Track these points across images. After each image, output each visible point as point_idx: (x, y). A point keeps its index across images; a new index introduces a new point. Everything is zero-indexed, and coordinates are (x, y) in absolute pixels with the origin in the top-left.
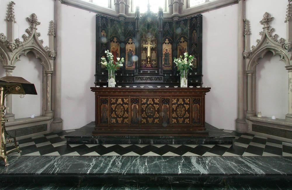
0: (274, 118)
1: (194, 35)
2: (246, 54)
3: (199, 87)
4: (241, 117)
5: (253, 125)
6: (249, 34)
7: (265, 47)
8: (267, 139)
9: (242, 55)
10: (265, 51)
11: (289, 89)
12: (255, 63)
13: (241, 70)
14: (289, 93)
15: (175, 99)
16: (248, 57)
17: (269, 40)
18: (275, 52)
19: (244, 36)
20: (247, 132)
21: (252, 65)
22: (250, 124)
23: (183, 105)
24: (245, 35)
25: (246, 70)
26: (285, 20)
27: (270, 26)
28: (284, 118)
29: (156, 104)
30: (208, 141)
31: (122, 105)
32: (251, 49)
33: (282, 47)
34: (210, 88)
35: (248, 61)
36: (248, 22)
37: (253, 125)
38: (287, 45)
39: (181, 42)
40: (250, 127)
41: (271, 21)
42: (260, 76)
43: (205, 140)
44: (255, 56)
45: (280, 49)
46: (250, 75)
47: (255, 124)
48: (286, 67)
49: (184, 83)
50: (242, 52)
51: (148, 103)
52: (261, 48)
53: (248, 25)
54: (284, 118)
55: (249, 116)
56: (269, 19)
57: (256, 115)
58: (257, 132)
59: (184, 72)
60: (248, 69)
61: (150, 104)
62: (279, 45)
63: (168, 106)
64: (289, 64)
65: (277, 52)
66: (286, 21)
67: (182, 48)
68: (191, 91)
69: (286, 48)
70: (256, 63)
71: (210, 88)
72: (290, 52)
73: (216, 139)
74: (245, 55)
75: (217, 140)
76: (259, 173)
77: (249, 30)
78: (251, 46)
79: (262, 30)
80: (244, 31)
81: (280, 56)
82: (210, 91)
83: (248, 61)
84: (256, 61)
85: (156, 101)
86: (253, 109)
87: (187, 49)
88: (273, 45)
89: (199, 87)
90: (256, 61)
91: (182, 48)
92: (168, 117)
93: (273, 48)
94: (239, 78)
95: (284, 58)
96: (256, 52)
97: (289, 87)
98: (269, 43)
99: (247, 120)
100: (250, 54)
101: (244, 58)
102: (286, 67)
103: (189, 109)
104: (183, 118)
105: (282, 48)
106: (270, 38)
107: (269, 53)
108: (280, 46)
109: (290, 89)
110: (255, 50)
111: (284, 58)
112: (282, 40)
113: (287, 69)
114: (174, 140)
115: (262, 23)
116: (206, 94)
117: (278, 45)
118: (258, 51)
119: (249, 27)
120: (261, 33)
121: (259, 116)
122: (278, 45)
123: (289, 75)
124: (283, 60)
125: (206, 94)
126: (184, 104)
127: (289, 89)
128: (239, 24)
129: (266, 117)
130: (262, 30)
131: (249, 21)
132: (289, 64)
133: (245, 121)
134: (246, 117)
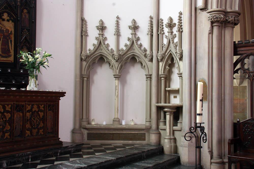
0: (104, 123)
1: (26, 16)
2: (84, 56)
3: (23, 89)
4: (77, 127)
5: (88, 133)
6: (87, 36)
7: (99, 53)
8: (100, 144)
9: (80, 57)
10: (99, 57)
11: (115, 95)
12: (90, 67)
13: (78, 72)
14: (115, 99)
15: (29, 105)
16: (85, 60)
17: (103, 48)
18: (107, 60)
19: (82, 36)
20: (83, 143)
21: (88, 69)
22: (86, 132)
23: (38, 112)
24: (83, 36)
25: (83, 73)
26: (114, 33)
27: (103, 34)
28: (112, 123)
29: (8, 112)
30: (63, 151)
31: (38, 112)
32: (88, 52)
33: (112, 57)
34: (65, 93)
35: (84, 63)
36: (86, 21)
37: (88, 133)
38: (116, 56)
39: (4, 20)
40: (85, 136)
41: (105, 29)
42: (93, 82)
43: (60, 151)
44: (91, 59)
45: (110, 58)
46: (85, 79)
47: (90, 132)
48: (114, 75)
49: (35, 85)
50: (80, 53)
51: (33, 110)
52: (96, 53)
53: (86, 25)
54: (112, 123)
55: (84, 124)
56: (104, 27)
57: (89, 123)
58: (91, 140)
59: (35, 71)
60: (84, 73)
61: (35, 111)
62: (110, 54)
63: (21, 114)
64: (116, 73)
65: (108, 60)
66: (115, 34)
67: (5, 30)
68: (22, 94)
69: (115, 58)
70: (91, 68)
71: (65, 93)
72: (117, 63)
73: (69, 148)
74: (83, 58)
75: (70, 149)
76: (113, 159)
77: (86, 32)
78: (88, 49)
79: (98, 36)
80: (82, 30)
81: (110, 64)
82: (65, 95)
83: (161, 64)
84: (91, 65)
85: (8, 108)
86: (87, 117)
87: (13, 33)
88: (106, 53)
89: (23, 89)
90: (91, 65)
91: (5, 30)
92: (20, 129)
93: (105, 55)
94: (76, 82)
95: (112, 67)
96: (92, 56)
97: (115, 93)
98: (102, 50)
99: (82, 130)
100: (87, 57)
101: (81, 59)
102: (114, 75)
103: (44, 116)
104: (37, 129)
105: (112, 58)
106: (104, 46)
107: (102, 59)
108: (111, 55)
109: (116, 95)
110: (92, 54)
111: (112, 67)
112: (112, 50)
113: (114, 77)
114: (30, 157)
115: (98, 28)
116: (60, 100)
117: (109, 54)
118: (94, 55)
119: (87, 28)
120: (97, 38)
121: (93, 123)
122: (109, 54)
123: (115, 83)
124: (112, 68)
125: (60, 100)
126: (31, 112)
127: (115, 95)
128: (77, 22)
129: (97, 124)
130: (98, 36)
131: (87, 21)
132: (116, 73)
133: (81, 131)
134: (82, 126)
